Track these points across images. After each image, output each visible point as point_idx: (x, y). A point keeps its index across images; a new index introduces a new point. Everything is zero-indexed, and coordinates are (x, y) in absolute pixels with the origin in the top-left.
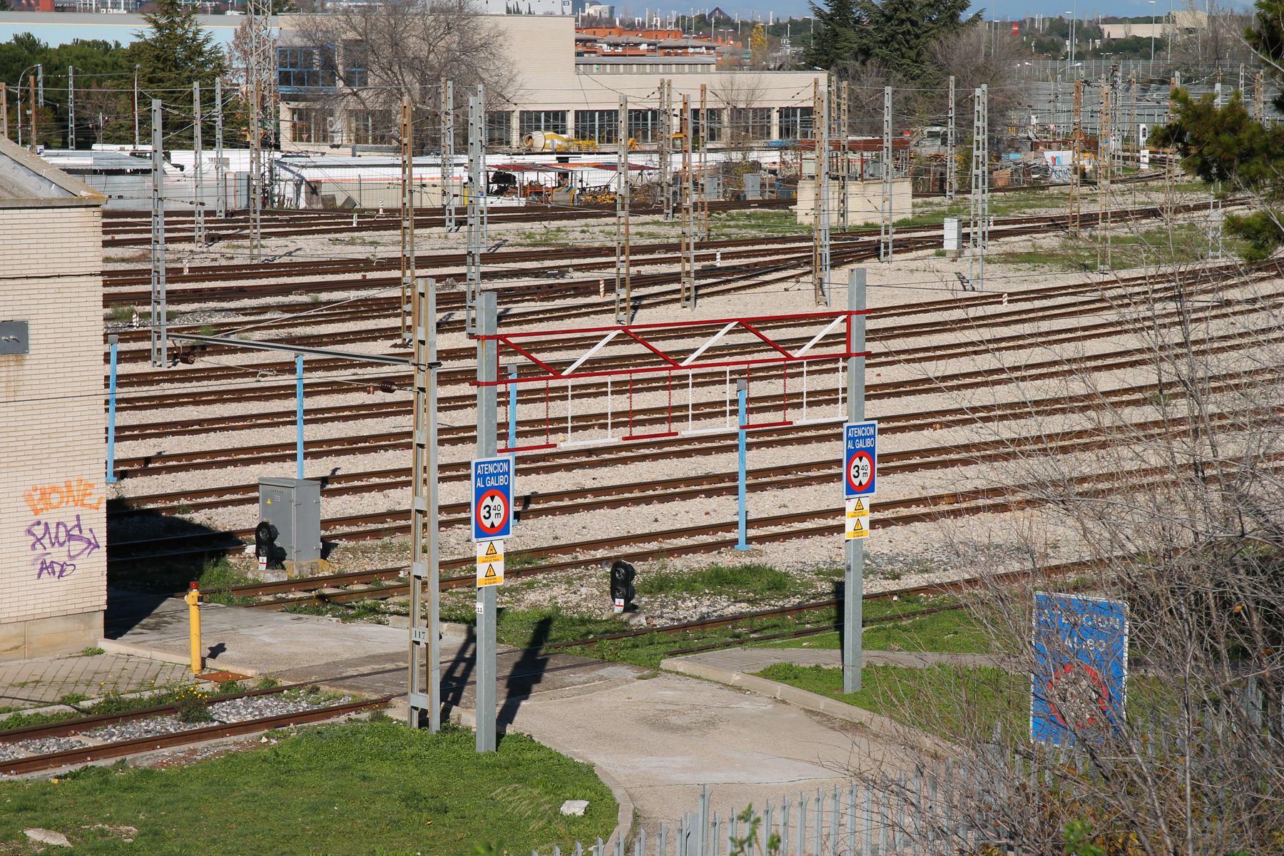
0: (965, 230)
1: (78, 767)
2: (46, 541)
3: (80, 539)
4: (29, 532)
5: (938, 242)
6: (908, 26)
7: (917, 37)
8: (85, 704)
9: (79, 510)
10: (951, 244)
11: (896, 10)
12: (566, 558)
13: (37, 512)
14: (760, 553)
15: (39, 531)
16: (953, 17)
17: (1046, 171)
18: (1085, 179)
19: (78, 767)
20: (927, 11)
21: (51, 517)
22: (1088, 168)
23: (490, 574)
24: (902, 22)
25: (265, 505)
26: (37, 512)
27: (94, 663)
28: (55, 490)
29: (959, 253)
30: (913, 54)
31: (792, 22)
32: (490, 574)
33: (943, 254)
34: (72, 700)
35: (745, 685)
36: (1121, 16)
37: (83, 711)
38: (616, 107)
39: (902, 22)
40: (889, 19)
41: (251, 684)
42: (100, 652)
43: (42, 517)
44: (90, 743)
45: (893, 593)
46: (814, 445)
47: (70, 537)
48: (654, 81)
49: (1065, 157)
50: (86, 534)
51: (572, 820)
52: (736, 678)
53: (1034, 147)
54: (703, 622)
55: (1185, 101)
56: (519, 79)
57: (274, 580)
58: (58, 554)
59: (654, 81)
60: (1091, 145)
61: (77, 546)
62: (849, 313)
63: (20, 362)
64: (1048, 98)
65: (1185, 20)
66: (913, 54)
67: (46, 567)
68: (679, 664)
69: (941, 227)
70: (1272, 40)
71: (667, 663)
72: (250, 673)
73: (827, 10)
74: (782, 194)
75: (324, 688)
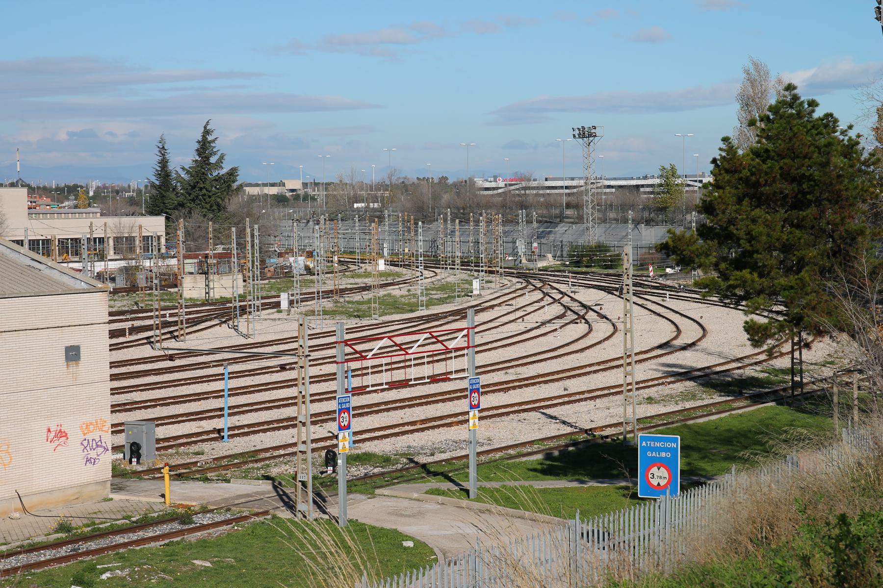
0: (292, 298)
1: (167, 541)
2: (88, 448)
3: (101, 446)
4: (82, 444)
5: (278, 305)
6: (204, 191)
7: (210, 197)
8: (134, 519)
9: (101, 433)
10: (284, 305)
11: (198, 182)
12: (268, 455)
13: (85, 434)
14: (360, 448)
15: (85, 443)
16: (229, 186)
17: (291, 267)
18: (309, 271)
19: (167, 541)
20: (214, 183)
21: (90, 437)
22: (311, 266)
23: (344, 448)
24: (201, 189)
25: (128, 433)
26: (85, 434)
27: (106, 506)
28: (91, 424)
29: (289, 311)
30: (208, 206)
31: (68, 187)
32: (344, 448)
33: (280, 312)
34: (127, 518)
35: (421, 498)
36: (254, 182)
37: (134, 522)
38: (23, 238)
39: (201, 189)
40: (194, 187)
41: (196, 509)
42: (112, 499)
43: (87, 437)
44: (122, 541)
45: (443, 461)
46: (325, 403)
47: (97, 446)
48: (87, 222)
49: (301, 260)
50: (104, 444)
51: (406, 548)
52: (415, 495)
53: (280, 255)
54: (366, 476)
55: (674, 233)
56: (7, 223)
57: (141, 469)
58: (93, 454)
59: (87, 222)
60: (310, 255)
61: (100, 450)
62: (468, 328)
63: (77, 365)
64: (291, 230)
65: (290, 185)
66: (208, 206)
67: (88, 460)
68: (385, 491)
69: (279, 296)
70: (785, 211)
71: (377, 491)
72: (194, 504)
73: (157, 183)
74: (171, 281)
75: (233, 508)
